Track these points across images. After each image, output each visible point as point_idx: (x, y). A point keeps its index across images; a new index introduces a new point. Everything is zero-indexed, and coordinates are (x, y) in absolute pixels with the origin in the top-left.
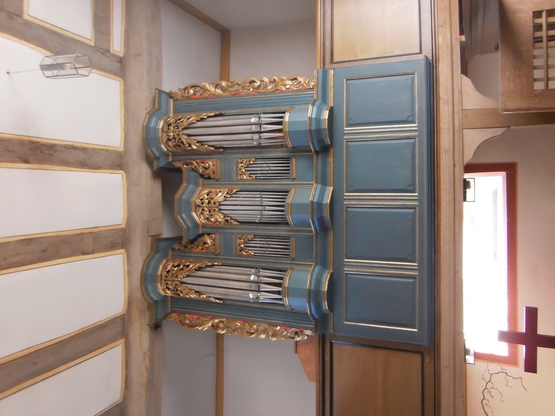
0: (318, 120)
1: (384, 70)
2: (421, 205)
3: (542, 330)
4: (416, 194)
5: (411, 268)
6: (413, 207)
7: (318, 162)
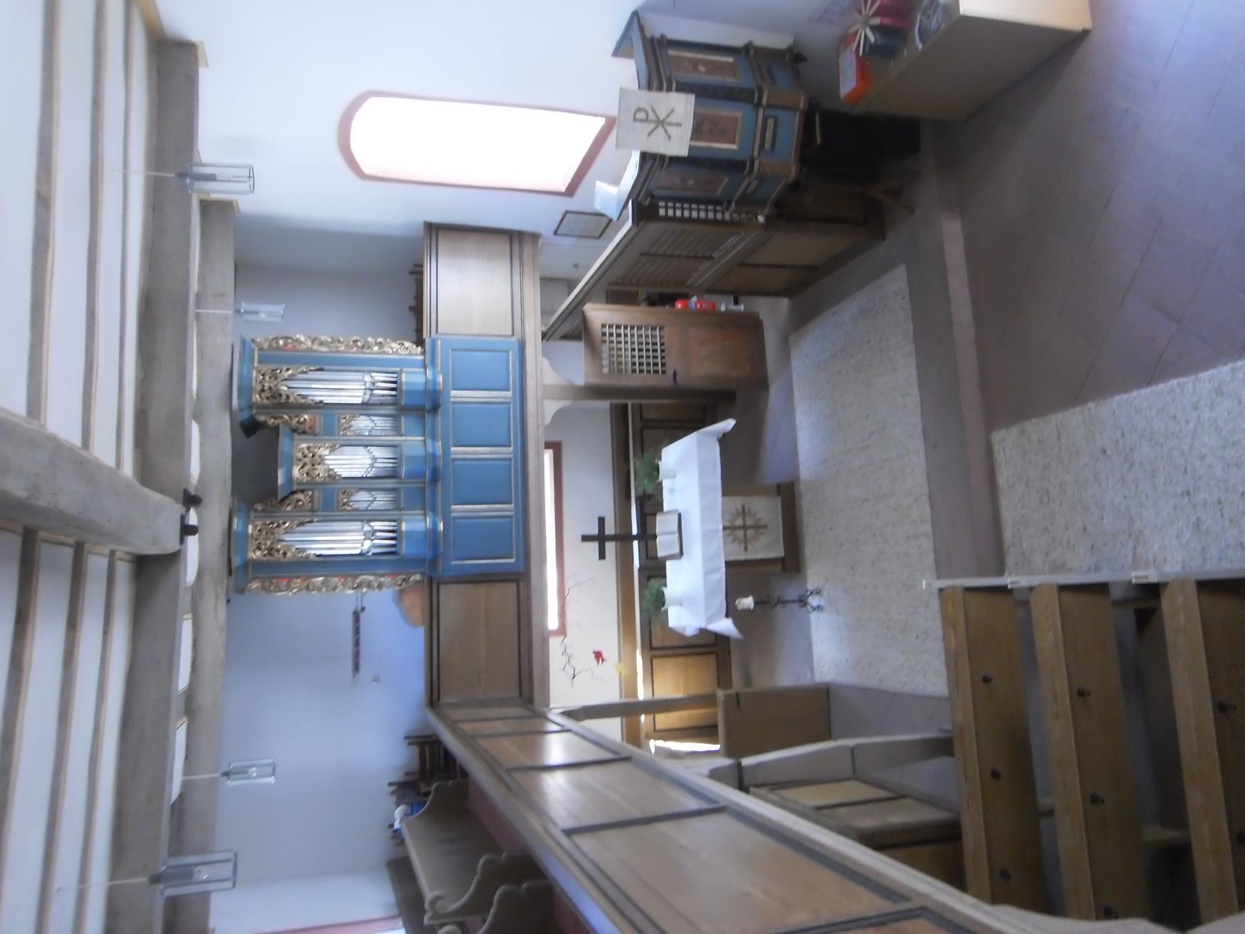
0: (435, 382)
1: (480, 346)
2: (516, 457)
3: (595, 531)
4: (513, 560)
5: (508, 508)
6: (510, 517)
7: (428, 419)
